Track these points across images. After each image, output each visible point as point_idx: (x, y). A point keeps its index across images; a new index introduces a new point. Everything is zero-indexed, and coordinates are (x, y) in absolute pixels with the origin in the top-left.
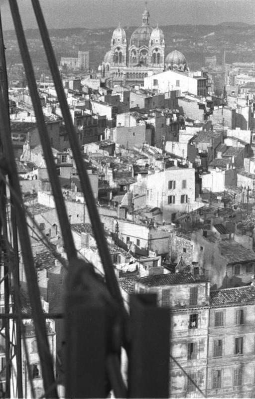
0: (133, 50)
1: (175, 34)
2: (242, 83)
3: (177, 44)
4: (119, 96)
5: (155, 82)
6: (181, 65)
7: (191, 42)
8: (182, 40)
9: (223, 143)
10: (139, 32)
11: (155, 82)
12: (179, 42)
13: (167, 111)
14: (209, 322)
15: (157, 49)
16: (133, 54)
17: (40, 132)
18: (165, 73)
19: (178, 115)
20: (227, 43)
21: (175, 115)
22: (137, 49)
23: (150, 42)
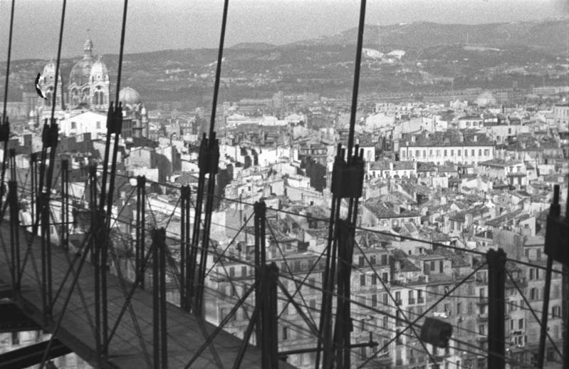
0: (74, 89)
1: (169, 62)
2: (234, 125)
3: (171, 77)
4: (17, 140)
5: (73, 125)
6: (135, 105)
7: (190, 73)
8: (178, 70)
9: (129, 182)
10: (80, 66)
11: (73, 125)
12: (174, 74)
13: (77, 155)
14: (437, 303)
15: (99, 87)
16: (74, 93)
17: (159, 171)
18: (84, 114)
19: (90, 158)
20: (242, 72)
21: (86, 159)
22: (78, 88)
23: (91, 78)
